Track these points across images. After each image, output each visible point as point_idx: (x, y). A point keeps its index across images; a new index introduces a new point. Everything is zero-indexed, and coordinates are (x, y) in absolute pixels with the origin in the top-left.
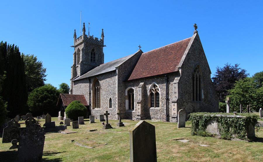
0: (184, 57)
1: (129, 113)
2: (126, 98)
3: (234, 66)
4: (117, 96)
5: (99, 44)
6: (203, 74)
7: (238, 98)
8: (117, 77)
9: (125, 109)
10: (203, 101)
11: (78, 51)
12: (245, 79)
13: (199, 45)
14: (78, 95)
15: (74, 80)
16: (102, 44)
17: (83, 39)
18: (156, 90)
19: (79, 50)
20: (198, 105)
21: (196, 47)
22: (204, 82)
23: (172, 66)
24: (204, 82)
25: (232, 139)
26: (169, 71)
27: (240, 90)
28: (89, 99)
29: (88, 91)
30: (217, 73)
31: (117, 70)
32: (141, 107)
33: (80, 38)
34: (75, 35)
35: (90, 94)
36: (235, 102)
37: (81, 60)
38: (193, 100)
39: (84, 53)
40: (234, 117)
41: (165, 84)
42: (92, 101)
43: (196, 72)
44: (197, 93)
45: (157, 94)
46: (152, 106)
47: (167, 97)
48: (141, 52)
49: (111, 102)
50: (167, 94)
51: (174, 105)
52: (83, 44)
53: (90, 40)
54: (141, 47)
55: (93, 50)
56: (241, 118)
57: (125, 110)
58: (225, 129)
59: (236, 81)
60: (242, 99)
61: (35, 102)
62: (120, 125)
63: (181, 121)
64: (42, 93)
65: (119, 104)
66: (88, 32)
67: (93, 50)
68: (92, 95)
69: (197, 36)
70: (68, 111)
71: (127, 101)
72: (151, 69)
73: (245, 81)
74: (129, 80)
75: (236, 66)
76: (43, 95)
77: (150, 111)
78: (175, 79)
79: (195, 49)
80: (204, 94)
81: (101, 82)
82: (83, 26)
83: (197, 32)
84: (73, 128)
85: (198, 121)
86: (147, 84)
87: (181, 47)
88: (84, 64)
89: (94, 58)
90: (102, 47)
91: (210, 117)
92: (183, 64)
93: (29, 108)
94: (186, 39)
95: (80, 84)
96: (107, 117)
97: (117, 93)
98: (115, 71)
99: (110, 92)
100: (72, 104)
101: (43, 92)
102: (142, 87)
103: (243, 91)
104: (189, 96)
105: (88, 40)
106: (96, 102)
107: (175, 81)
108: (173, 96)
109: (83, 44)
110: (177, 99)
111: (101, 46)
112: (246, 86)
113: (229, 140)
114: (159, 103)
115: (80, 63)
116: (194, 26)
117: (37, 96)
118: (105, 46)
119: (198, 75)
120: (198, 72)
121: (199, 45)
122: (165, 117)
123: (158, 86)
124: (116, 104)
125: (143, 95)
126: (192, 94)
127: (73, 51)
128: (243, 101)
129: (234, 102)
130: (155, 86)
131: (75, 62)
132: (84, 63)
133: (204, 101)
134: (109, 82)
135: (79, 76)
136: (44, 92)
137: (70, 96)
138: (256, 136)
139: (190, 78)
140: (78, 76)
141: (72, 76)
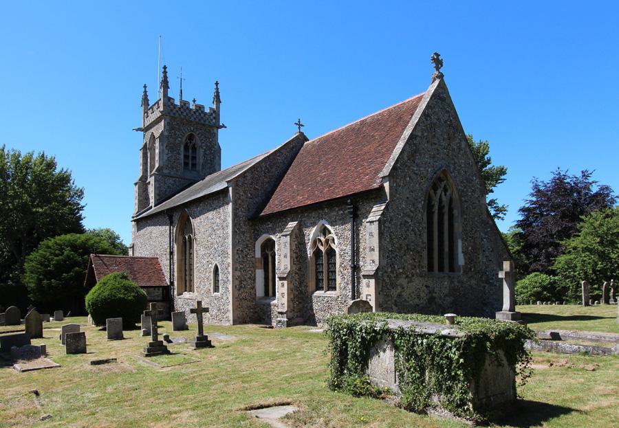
0: (400, 145)
2: (257, 265)
3: (579, 175)
4: (230, 260)
6: (460, 196)
7: (589, 263)
8: (229, 208)
9: (255, 294)
10: (462, 271)
11: (152, 141)
12: (608, 211)
13: (448, 112)
14: (142, 258)
16: (214, 121)
17: (162, 110)
20: (446, 283)
21: (438, 119)
22: (465, 219)
25: (430, 411)
26: (359, 188)
27: (594, 242)
30: (534, 196)
31: (230, 189)
33: (155, 108)
34: (145, 100)
36: (581, 274)
37: (157, 165)
38: (430, 268)
39: (165, 146)
40: (433, 335)
41: (349, 226)
42: (176, 274)
43: (439, 192)
45: (331, 253)
46: (318, 288)
47: (353, 263)
48: (302, 139)
50: (356, 253)
53: (182, 110)
55: (191, 138)
56: (452, 338)
57: (254, 299)
58: (413, 373)
59: (583, 217)
60: (600, 266)
61: (41, 277)
62: (196, 344)
64: (57, 252)
65: (237, 282)
66: (179, 91)
67: (191, 138)
69: (442, 88)
70: (90, 303)
71: (260, 274)
72: (317, 183)
73: (607, 216)
74: (262, 214)
75: (585, 175)
76: (61, 257)
77: (315, 300)
78: (373, 210)
79: (435, 124)
81: (195, 222)
82: (162, 75)
83: (441, 76)
84: (67, 353)
85: (344, 343)
86: (307, 227)
87: (398, 118)
88: (166, 176)
89: (194, 158)
90: (215, 130)
91: (375, 331)
93: (29, 293)
94: (412, 98)
95: (150, 229)
97: (230, 251)
98: (225, 191)
100: (104, 283)
101: (61, 250)
102: (291, 235)
103: (601, 243)
104: (414, 259)
106: (186, 275)
107: (371, 214)
110: (375, 269)
111: (212, 127)
112: (609, 229)
113: (420, 412)
114: (335, 280)
115: (154, 172)
116: (433, 59)
117: (44, 263)
118: (223, 126)
119: (444, 198)
120: (445, 190)
123: (332, 231)
124: (228, 280)
125: (294, 255)
126: (425, 253)
127: (140, 140)
128: (603, 271)
129: (579, 274)
130: (325, 231)
131: (145, 170)
132: (166, 171)
133: (465, 271)
136: (63, 249)
138: (518, 398)
139: (420, 206)
141: (137, 207)
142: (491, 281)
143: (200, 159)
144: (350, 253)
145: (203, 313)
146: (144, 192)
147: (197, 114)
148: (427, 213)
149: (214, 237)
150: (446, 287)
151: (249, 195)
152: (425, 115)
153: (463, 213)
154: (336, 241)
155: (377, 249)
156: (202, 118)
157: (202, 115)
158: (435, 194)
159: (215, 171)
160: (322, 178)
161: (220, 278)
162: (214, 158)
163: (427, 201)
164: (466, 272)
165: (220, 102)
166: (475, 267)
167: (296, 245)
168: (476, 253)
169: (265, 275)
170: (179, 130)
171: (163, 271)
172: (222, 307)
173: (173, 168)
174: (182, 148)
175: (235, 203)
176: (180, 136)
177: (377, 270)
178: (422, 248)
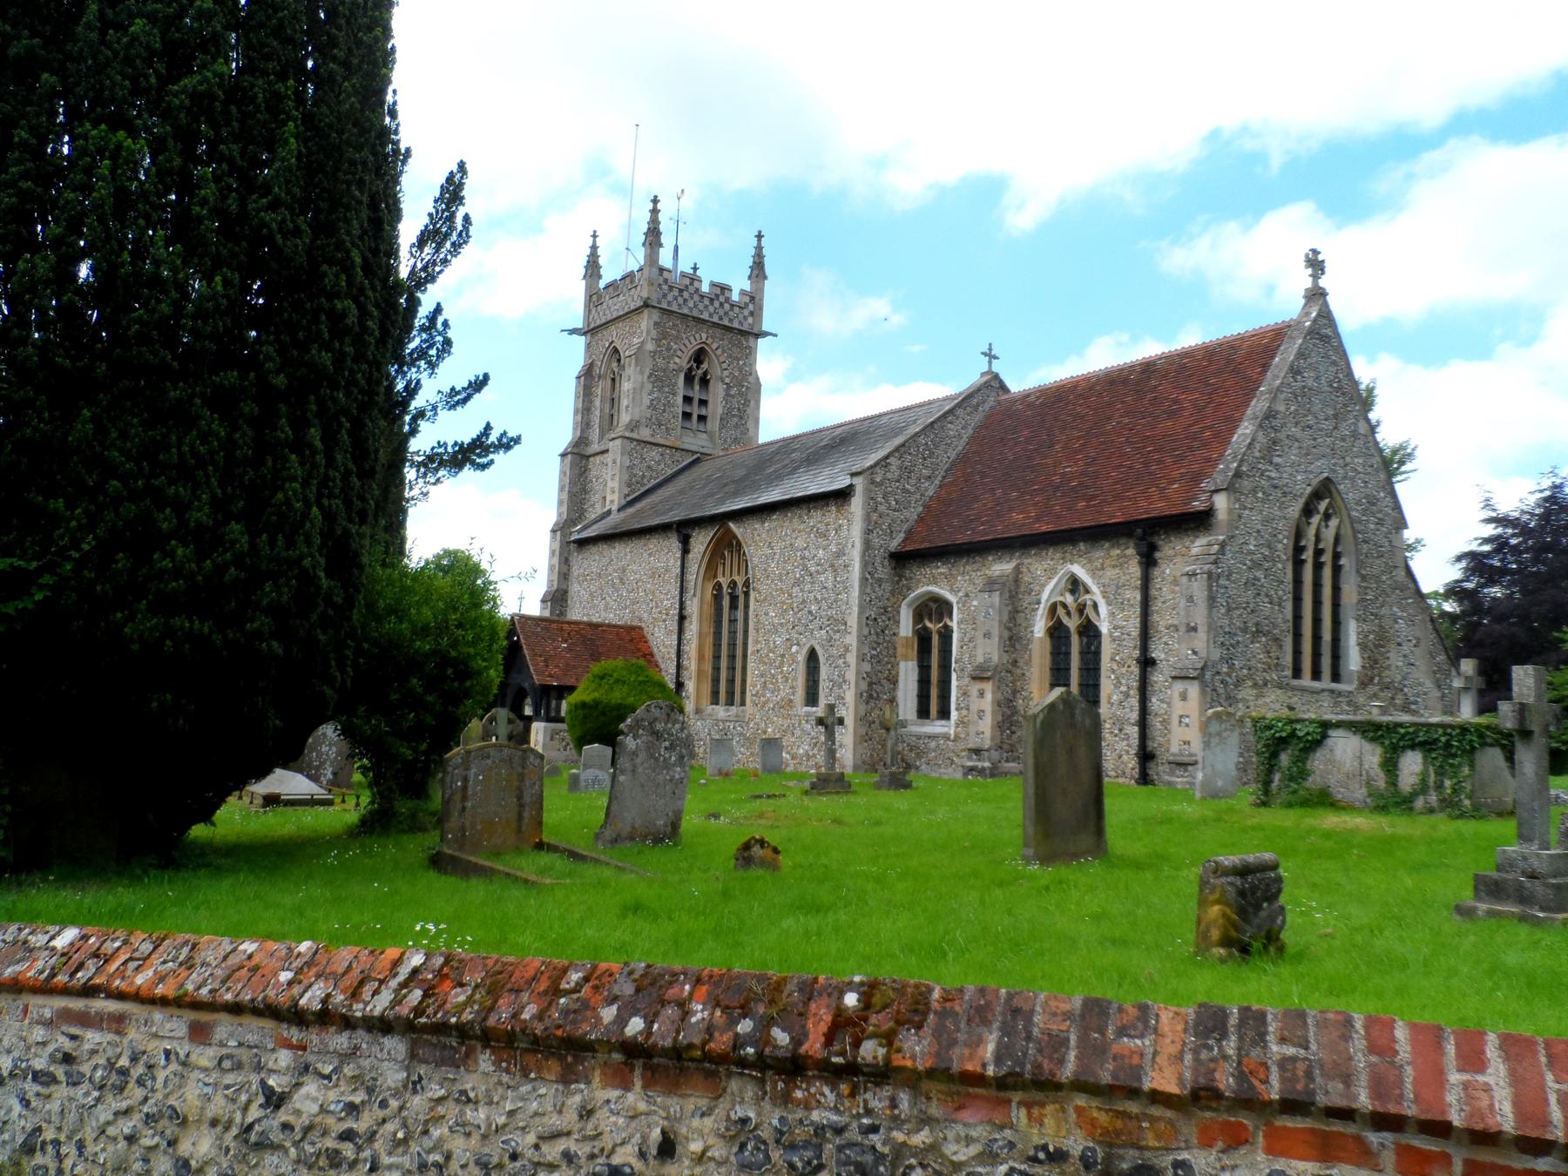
1: (919, 737)
2: (900, 651)
4: (852, 640)
5: (736, 325)
6: (1355, 532)
16: (750, 320)
23: (1175, 482)
24: (1364, 578)
26: (1159, 508)
29: (670, 602)
31: (859, 490)
35: (682, 618)
38: (1297, 673)
39: (647, 373)
43: (1315, 520)
44: (1317, 638)
45: (1090, 632)
51: (1184, 697)
55: (699, 356)
65: (864, 686)
68: (692, 628)
71: (908, 673)
80: (1363, 646)
89: (703, 403)
97: (853, 621)
104: (1269, 652)
105: (676, 299)
120: (1327, 517)
121: (1334, 363)
123: (1094, 588)
132: (645, 433)
135: (609, 512)
137: (566, 627)
140: (599, 510)
142: (1413, 707)
143: (716, 408)
144: (1135, 633)
147: (717, 304)
153: (1360, 565)
154: (1103, 609)
155: (1202, 629)
157: (727, 306)
162: (747, 403)
163: (1293, 539)
164: (1364, 683)
170: (677, 338)
173: (660, 425)
176: (679, 353)
178: (1282, 631)
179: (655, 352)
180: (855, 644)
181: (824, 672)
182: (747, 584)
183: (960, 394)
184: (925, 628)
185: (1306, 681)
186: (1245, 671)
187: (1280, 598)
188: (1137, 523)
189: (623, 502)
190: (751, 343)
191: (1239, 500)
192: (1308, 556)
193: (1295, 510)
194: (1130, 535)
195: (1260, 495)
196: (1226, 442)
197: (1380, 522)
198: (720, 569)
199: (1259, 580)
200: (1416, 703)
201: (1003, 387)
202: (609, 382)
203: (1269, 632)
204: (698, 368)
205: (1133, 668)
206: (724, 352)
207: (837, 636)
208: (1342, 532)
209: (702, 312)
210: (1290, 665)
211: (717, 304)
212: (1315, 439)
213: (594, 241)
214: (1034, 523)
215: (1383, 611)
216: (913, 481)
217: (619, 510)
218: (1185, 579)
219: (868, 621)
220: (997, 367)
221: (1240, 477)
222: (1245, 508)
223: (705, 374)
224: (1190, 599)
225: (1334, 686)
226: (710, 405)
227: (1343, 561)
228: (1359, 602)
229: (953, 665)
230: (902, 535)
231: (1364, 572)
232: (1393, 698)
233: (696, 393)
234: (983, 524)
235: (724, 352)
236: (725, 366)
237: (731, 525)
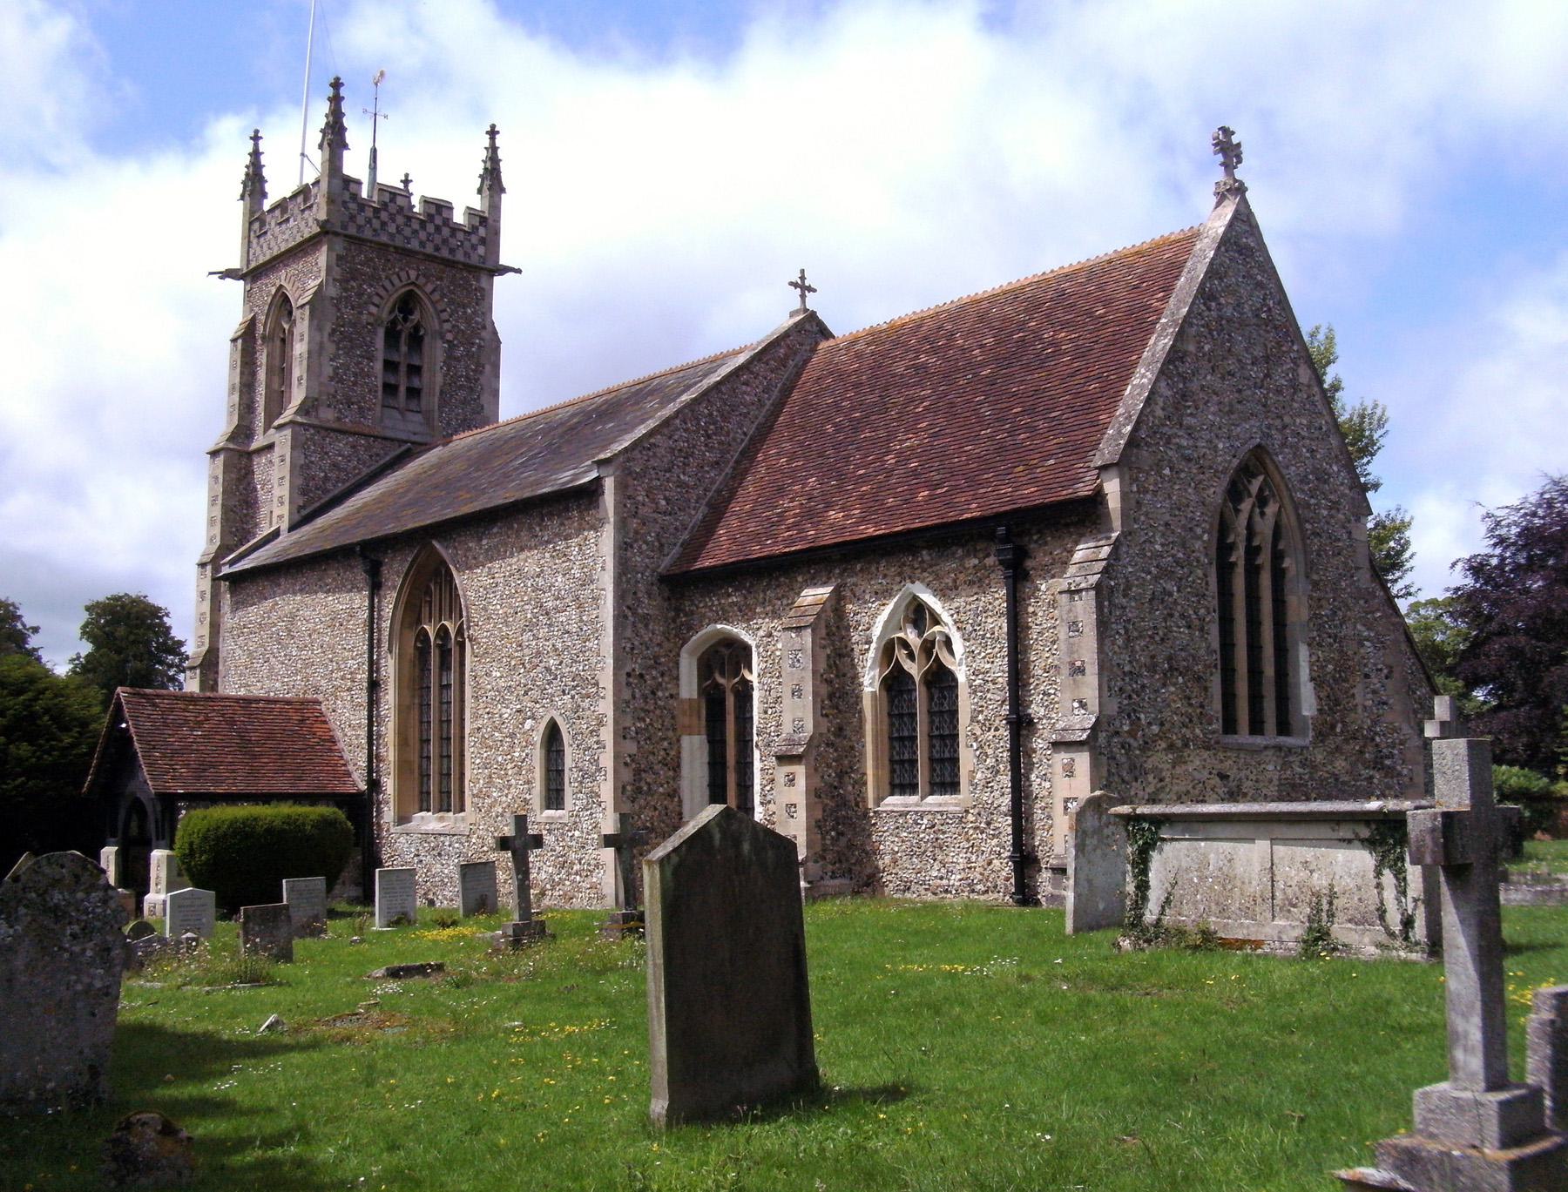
0: (1142, 378)
2: (684, 720)
4: (606, 707)
5: (460, 257)
6: (1301, 521)
8: (603, 544)
10: (1311, 733)
13: (1260, 285)
15: (232, 563)
16: (481, 250)
18: (928, 647)
19: (282, 303)
20: (1271, 767)
24: (1315, 584)
26: (1030, 494)
28: (363, 733)
29: (357, 663)
31: (609, 484)
32: (814, 794)
35: (374, 686)
37: (298, 396)
38: (1230, 726)
39: (328, 328)
43: (1246, 506)
45: (941, 680)
49: (561, 753)
52: (322, 257)
53: (384, 215)
54: (810, 289)
55: (407, 304)
63: (1090, 881)
65: (627, 775)
68: (389, 698)
71: (694, 750)
72: (890, 473)
78: (1078, 556)
81: (471, 583)
83: (1239, 190)
86: (856, 597)
89: (415, 370)
92: (1133, 442)
96: (522, 868)
97: (607, 679)
99: (548, 669)
102: (814, 627)
105: (369, 221)
107: (1072, 570)
108: (1065, 699)
109: (322, 257)
115: (288, 415)
120: (1262, 501)
122: (1004, 869)
125: (824, 690)
132: (327, 415)
134: (541, 581)
135: (276, 534)
139: (1198, 545)
140: (265, 531)
142: (1388, 762)
143: (435, 376)
144: (1003, 680)
145: (296, 938)
146: (239, 480)
147: (431, 228)
148: (1218, 569)
149: (543, 632)
150: (1271, 781)
151: (663, 502)
152: (1205, 295)
153: (1311, 567)
154: (958, 645)
155: (1092, 670)
156: (445, 241)
157: (446, 232)
158: (1237, 511)
159: (486, 422)
160: (903, 457)
161: (568, 762)
162: (479, 369)
163: (1215, 534)
164: (1321, 736)
165: (503, 190)
166: (1343, 722)
167: (828, 656)
168: (1346, 680)
169: (712, 754)
170: (374, 279)
171: (341, 745)
172: (573, 856)
173: (349, 404)
174: (380, 341)
175: (621, 526)
176: (376, 300)
177: (1094, 728)
178: (1207, 667)
179: (339, 299)
180: (610, 714)
181: (570, 756)
182: (460, 632)
183: (763, 341)
184: (717, 686)
185: (1243, 737)
186: (1155, 729)
187: (1202, 619)
188: (998, 518)
189: (297, 518)
190: (484, 283)
191: (1137, 479)
192: (1238, 556)
193: (1216, 492)
194: (991, 537)
195: (1167, 471)
196: (1118, 393)
197: (1335, 506)
198: (425, 611)
199: (1170, 594)
200: (1391, 756)
201: (825, 333)
202: (278, 343)
203: (1188, 669)
204: (405, 319)
205: (1001, 731)
206: (443, 296)
207: (586, 704)
208: (1284, 520)
209: (408, 240)
210: (1220, 715)
211: (431, 228)
212: (1239, 391)
213: (256, 146)
214: (857, 524)
215: (1346, 631)
216: (691, 470)
217: (292, 529)
218: (1065, 598)
219: (626, 679)
220: (812, 302)
221: (1138, 446)
222: (1146, 491)
223: (417, 328)
224: (1074, 626)
225: (1282, 740)
226: (426, 374)
227: (1287, 563)
228: (1311, 619)
229: (755, 738)
230: (676, 550)
231: (1315, 577)
232: (1361, 752)
233: (402, 354)
234: (788, 529)
235: (443, 296)
236: (445, 316)
237: (435, 543)
